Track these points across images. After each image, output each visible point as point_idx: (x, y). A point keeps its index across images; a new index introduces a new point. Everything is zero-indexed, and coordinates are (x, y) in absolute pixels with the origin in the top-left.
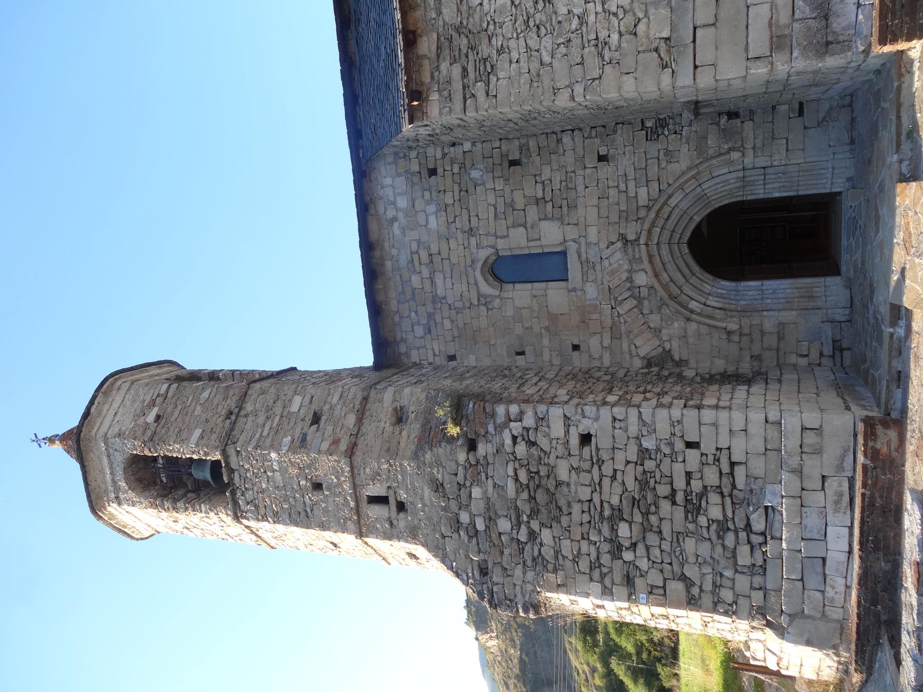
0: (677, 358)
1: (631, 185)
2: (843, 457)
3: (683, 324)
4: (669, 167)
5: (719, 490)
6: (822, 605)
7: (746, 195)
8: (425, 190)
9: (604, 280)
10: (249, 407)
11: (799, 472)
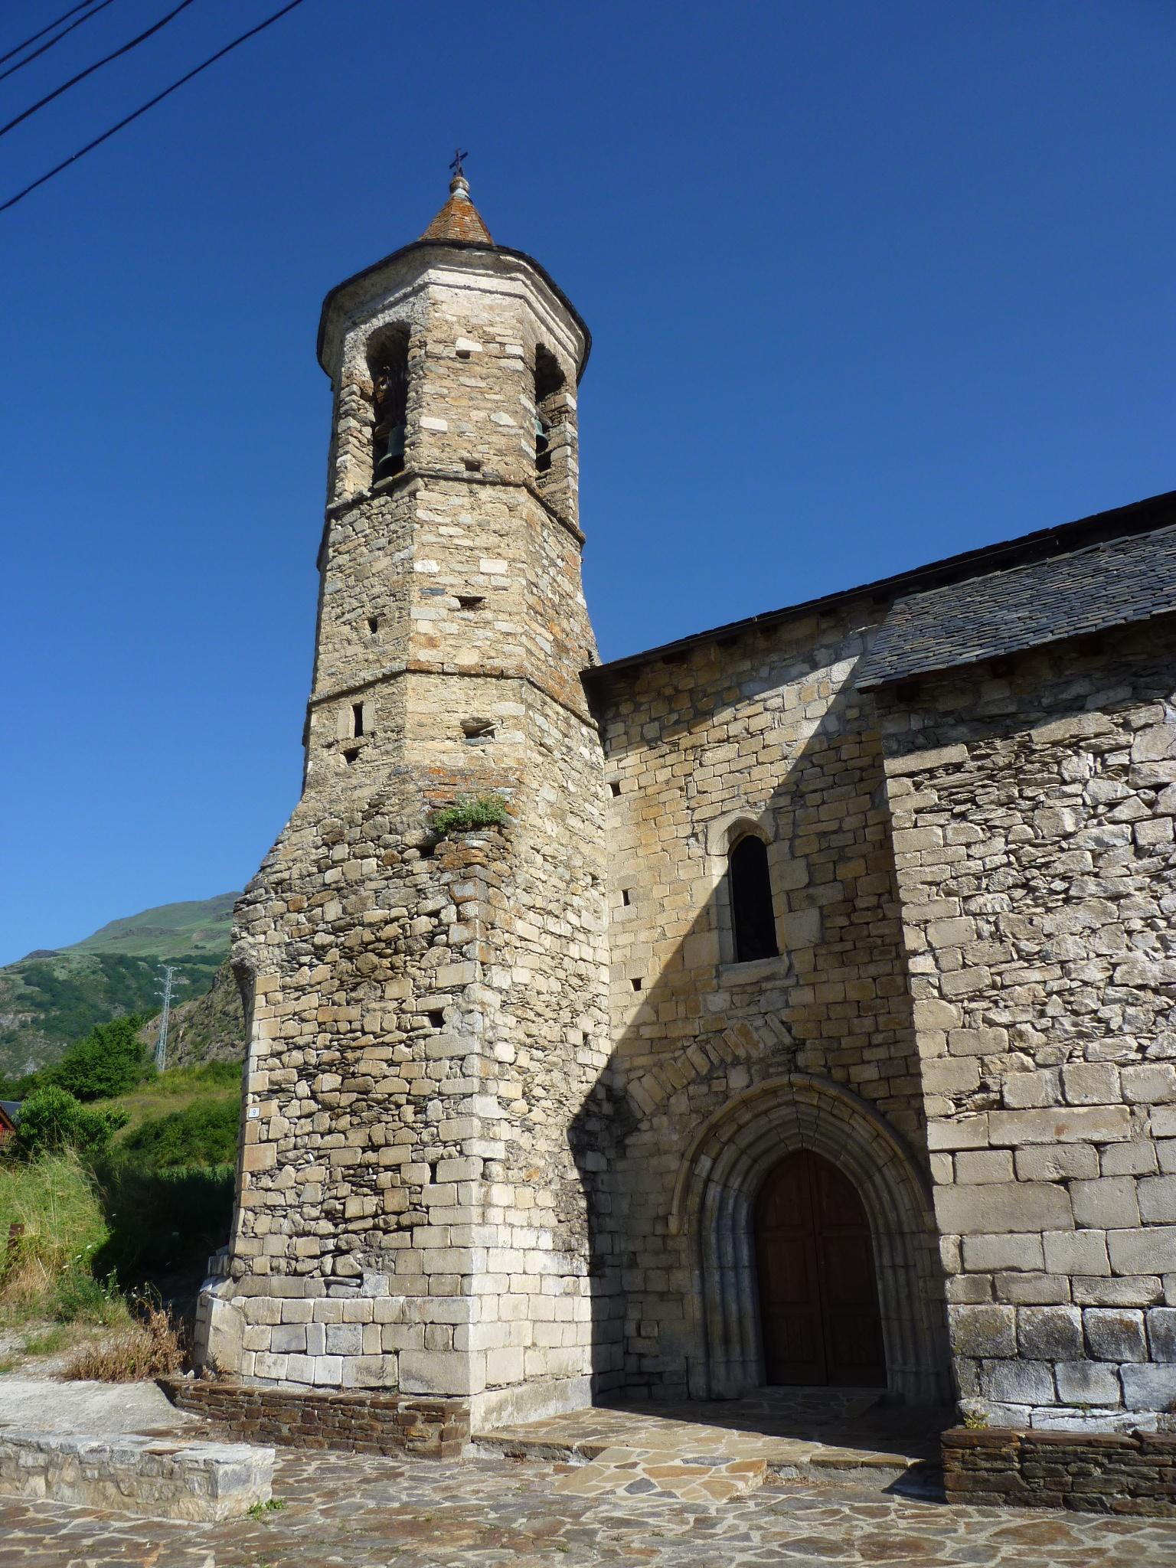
0: (628, 1141)
1: (881, 1053)
2: (420, 1379)
5: (380, 1212)
6: (256, 1348)
8: (861, 710)
9: (735, 1020)
10: (485, 493)
11: (402, 1321)
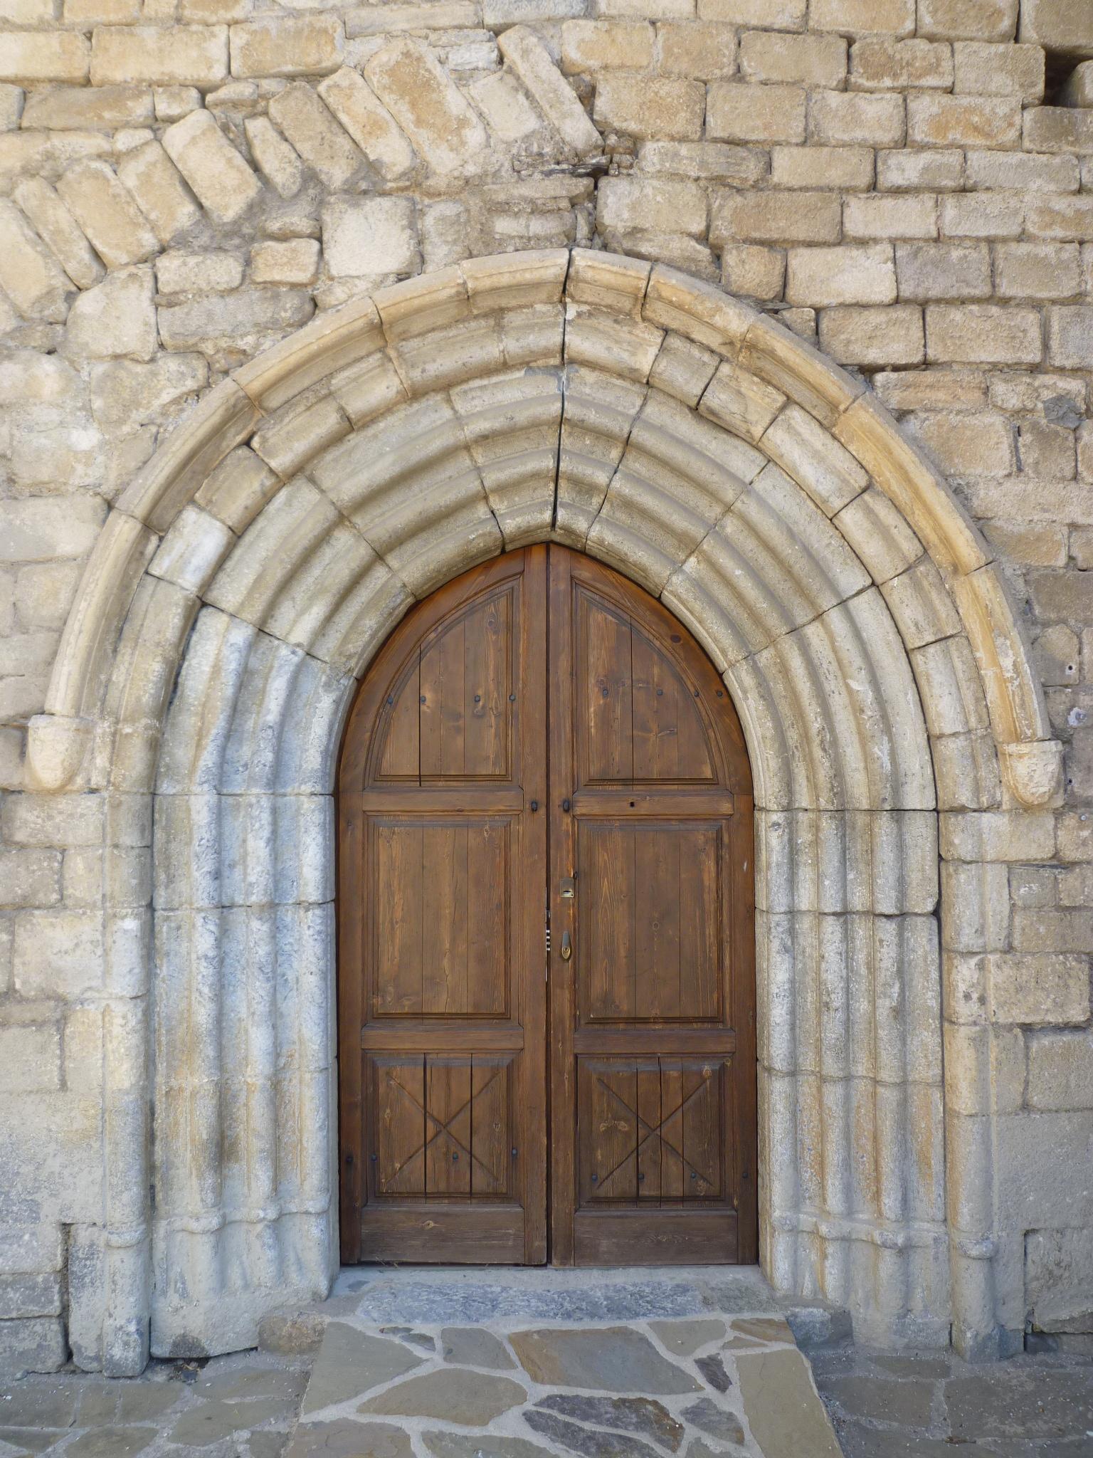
3: (82, 475)
4: (996, 421)
7: (791, 825)
